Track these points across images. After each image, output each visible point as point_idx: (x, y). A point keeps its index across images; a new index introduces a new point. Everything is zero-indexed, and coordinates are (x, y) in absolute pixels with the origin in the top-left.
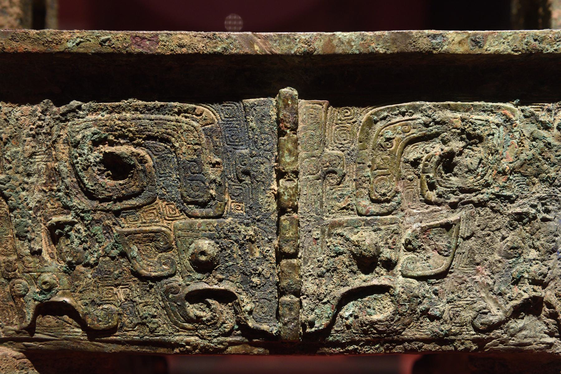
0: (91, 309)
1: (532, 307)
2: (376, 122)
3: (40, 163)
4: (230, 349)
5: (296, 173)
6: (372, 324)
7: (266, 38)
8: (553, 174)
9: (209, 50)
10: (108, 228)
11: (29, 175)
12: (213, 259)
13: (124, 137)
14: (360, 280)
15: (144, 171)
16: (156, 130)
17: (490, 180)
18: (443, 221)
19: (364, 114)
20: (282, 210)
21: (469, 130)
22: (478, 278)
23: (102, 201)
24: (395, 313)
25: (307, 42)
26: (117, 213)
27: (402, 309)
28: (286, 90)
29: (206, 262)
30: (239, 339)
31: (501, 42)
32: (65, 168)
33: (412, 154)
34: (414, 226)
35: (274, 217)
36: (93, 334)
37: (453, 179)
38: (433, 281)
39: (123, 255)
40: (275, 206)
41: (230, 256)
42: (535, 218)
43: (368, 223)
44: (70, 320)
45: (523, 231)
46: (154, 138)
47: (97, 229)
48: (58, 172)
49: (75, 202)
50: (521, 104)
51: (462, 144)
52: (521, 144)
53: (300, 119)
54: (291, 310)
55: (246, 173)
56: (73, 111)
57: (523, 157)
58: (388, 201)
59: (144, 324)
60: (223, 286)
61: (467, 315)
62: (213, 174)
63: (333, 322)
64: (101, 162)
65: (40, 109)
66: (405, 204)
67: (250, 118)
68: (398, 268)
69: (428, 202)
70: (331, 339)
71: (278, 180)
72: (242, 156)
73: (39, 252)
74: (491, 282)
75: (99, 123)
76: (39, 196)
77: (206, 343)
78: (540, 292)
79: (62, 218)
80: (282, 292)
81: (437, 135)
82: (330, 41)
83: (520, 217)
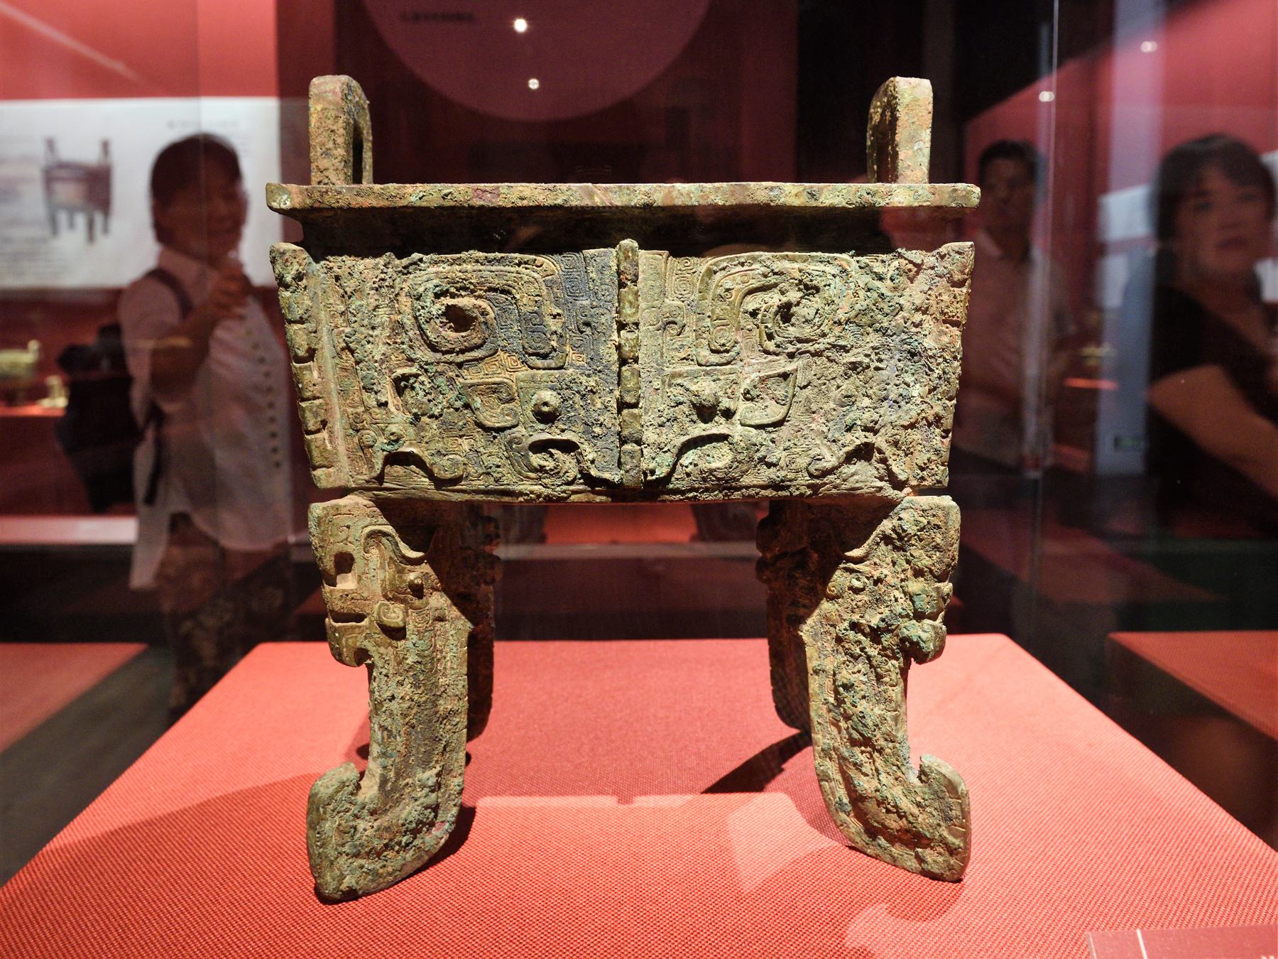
0: (437, 459)
1: (863, 452)
2: (715, 272)
3: (383, 316)
4: (573, 498)
5: (637, 324)
6: (711, 471)
7: (606, 189)
8: (885, 324)
9: (550, 202)
10: (451, 380)
11: (373, 328)
12: (556, 410)
13: (465, 289)
14: (700, 429)
15: (486, 323)
16: (497, 282)
17: (827, 331)
18: (781, 370)
19: (702, 264)
20: (623, 361)
21: (806, 281)
22: (813, 426)
23: (444, 353)
24: (734, 460)
25: (647, 194)
26: (460, 365)
27: (740, 457)
28: (627, 242)
29: (549, 413)
30: (581, 487)
31: (836, 195)
32: (408, 321)
33: (752, 303)
34: (753, 376)
35: (615, 368)
36: (440, 483)
37: (790, 328)
38: (771, 429)
39: (467, 406)
40: (616, 357)
41: (572, 406)
42: (868, 367)
43: (707, 373)
44: (418, 470)
45: (856, 380)
46: (495, 290)
47: (440, 381)
48: (402, 326)
49: (419, 354)
50: (857, 255)
51: (800, 294)
52: (856, 294)
53: (640, 269)
54: (632, 457)
55: (587, 324)
56: (415, 263)
57: (858, 307)
58: (727, 351)
59: (488, 474)
60: (565, 436)
61: (802, 462)
62: (554, 325)
63: (673, 470)
64: (444, 314)
65: (382, 262)
66: (744, 354)
67: (590, 269)
68: (737, 417)
69: (767, 352)
70: (671, 486)
71: (619, 330)
72: (583, 307)
73: (386, 404)
74: (825, 430)
75: (441, 275)
76: (383, 348)
77: (550, 491)
78: (871, 438)
79: (407, 371)
80: (623, 441)
81: (776, 285)
82: (670, 192)
83: (854, 366)
